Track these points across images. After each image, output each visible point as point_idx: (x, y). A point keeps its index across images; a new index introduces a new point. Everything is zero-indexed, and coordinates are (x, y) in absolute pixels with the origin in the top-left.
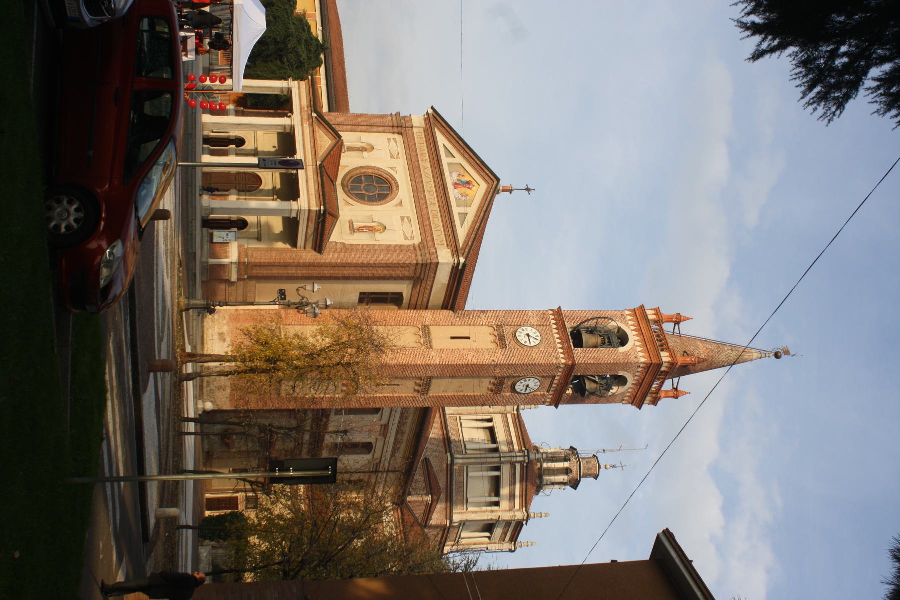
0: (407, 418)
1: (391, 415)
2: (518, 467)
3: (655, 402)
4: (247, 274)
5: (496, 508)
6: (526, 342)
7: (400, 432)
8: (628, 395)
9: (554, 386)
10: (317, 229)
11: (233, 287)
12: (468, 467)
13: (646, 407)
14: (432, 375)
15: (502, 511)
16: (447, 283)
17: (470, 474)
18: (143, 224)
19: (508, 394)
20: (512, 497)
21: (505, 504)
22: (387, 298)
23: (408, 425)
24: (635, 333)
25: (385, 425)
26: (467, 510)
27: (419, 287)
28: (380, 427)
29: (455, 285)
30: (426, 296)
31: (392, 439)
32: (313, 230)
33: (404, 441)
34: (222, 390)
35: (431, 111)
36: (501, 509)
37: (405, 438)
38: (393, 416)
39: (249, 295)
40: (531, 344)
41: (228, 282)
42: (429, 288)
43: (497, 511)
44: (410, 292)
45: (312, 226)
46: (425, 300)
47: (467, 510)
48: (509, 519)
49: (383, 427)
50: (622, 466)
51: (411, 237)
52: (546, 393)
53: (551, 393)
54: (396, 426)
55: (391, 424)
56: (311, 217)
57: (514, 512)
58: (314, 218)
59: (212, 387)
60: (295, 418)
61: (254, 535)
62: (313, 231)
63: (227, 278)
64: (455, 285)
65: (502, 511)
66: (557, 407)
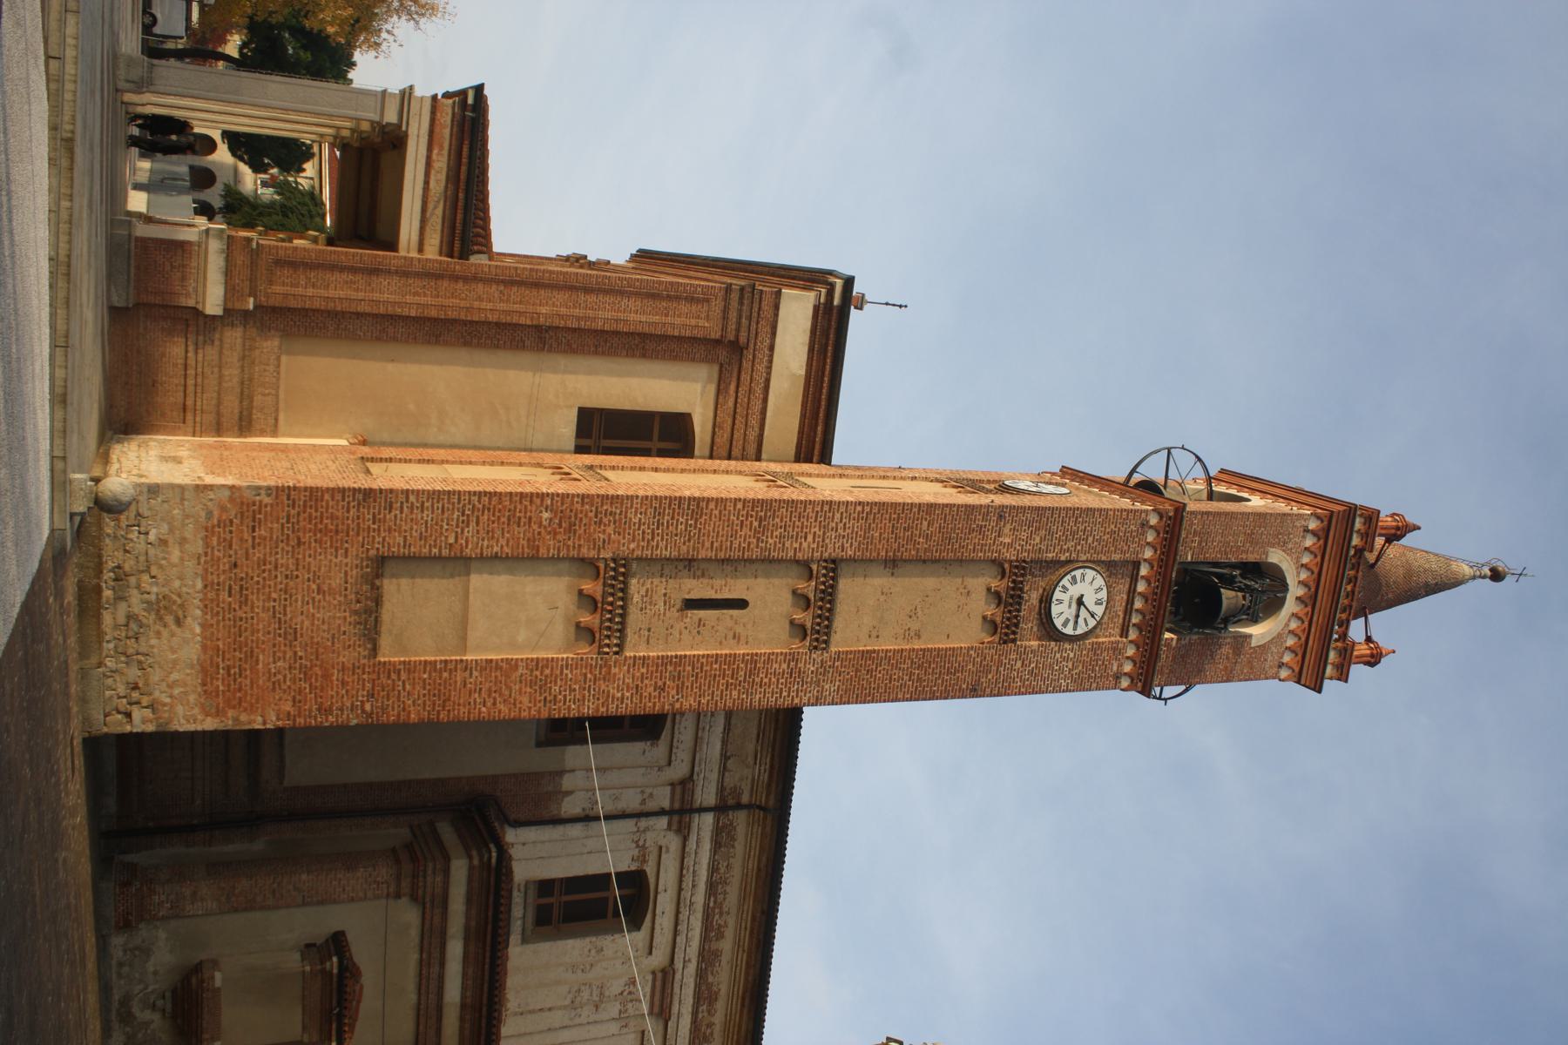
0: (720, 936)
3: (1343, 675)
4: (253, 293)
6: (1065, 624)
7: (704, 995)
8: (1290, 642)
9: (1138, 604)
10: (453, 177)
11: (209, 349)
13: (1328, 685)
14: (838, 554)
16: (803, 372)
19: (1035, 643)
22: (661, 439)
23: (724, 962)
24: (1301, 592)
25: (663, 971)
27: (733, 387)
28: (650, 977)
29: (828, 367)
30: (754, 422)
31: (686, 1022)
32: (443, 177)
33: (717, 1029)
34: (169, 619)
37: (718, 1019)
38: (682, 928)
39: (258, 400)
40: (1075, 629)
41: (194, 322)
42: (759, 391)
44: (711, 414)
45: (441, 163)
46: (752, 435)
49: (659, 975)
50: (1520, 575)
51: (587, 791)
52: (1118, 638)
53: (1133, 635)
54: (692, 968)
55: (678, 965)
56: (437, 130)
58: (447, 132)
59: (136, 603)
60: (414, 898)
62: (443, 184)
63: (191, 303)
64: (828, 367)
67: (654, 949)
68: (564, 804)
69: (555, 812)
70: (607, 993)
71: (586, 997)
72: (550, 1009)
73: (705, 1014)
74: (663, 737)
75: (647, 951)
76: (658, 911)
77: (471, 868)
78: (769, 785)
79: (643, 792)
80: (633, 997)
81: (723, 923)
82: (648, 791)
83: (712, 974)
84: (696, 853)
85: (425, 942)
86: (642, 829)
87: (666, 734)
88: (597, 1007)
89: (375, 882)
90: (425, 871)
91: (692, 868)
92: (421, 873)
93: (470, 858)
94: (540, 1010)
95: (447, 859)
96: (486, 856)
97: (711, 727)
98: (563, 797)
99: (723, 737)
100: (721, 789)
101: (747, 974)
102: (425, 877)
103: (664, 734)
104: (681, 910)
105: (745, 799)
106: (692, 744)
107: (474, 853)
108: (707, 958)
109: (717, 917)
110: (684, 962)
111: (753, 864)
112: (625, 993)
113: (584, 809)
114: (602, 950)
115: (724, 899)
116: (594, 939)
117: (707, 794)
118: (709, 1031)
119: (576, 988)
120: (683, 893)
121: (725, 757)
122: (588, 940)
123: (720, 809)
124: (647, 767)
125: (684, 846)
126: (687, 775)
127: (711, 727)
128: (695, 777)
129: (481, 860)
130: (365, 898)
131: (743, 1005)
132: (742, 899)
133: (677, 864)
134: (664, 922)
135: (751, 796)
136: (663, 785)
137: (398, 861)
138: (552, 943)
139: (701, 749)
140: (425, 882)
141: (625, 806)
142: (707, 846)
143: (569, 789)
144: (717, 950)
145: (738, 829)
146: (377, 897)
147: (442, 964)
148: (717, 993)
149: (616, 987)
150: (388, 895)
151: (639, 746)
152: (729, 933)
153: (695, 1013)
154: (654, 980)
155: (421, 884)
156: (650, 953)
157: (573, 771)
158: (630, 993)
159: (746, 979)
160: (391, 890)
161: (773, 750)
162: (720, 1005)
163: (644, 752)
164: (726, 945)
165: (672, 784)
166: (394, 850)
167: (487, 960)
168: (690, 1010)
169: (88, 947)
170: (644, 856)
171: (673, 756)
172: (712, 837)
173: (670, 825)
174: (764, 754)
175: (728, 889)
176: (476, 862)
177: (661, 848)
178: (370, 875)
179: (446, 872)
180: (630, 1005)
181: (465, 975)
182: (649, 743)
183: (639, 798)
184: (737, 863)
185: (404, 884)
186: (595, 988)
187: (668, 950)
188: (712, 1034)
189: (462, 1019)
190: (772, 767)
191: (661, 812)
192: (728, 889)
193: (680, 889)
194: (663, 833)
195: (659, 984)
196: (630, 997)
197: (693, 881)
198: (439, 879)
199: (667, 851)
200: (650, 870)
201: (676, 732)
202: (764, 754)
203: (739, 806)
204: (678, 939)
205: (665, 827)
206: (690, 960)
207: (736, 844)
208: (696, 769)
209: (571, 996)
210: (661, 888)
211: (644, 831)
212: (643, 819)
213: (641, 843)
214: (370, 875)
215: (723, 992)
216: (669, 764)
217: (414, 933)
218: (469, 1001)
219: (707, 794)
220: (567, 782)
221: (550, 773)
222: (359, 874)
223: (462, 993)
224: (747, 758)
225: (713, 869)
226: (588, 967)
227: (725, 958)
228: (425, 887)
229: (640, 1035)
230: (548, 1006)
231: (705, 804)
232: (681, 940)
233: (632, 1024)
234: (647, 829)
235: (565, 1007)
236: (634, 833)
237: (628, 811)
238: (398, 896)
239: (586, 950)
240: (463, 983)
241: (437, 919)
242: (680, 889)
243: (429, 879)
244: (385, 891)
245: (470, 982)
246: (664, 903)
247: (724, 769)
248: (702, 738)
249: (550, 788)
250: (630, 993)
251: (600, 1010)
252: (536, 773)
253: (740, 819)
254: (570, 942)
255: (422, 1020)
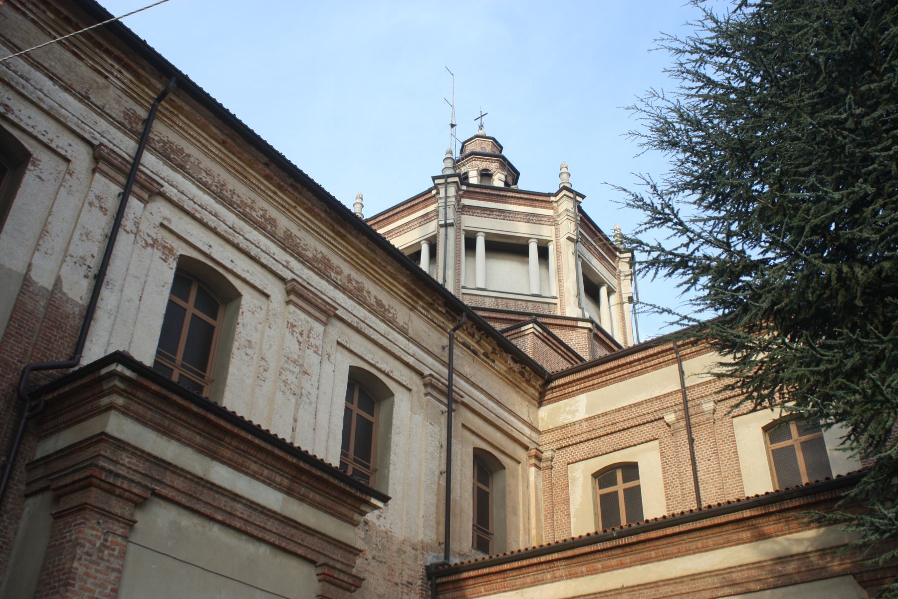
0: (273, 222)
1: (187, 213)
2: (466, 202)
5: (552, 248)
7: (322, 268)
12: (464, 287)
15: (557, 236)
17: (480, 285)
18: (808, 539)
20: (529, 218)
21: (547, 232)
25: (288, 292)
26: (555, 298)
28: (292, 308)
31: (341, 298)
33: (355, 275)
35: (320, 577)
36: (553, 238)
37: (347, 269)
38: (254, 251)
43: (558, 247)
47: (555, 298)
48: (573, 224)
49: (292, 297)
54: (295, 264)
55: (288, 275)
57: (559, 216)
60: (140, 503)
61: (761, 284)
65: (557, 236)
66: (389, 498)
67: (265, 291)
68: (70, 295)
69: (77, 310)
70: (296, 357)
71: (293, 379)
72: (295, 420)
73: (339, 277)
74: (30, 149)
75: (263, 299)
76: (229, 266)
77: (125, 412)
78: (137, 76)
79: (91, 204)
80: (305, 333)
81: (261, 212)
82: (91, 197)
83: (306, 250)
84: (182, 193)
85: (203, 509)
86: (135, 230)
87: (28, 144)
88: (305, 373)
89: (100, 550)
90: (110, 472)
91: (196, 206)
92: (111, 480)
93: (111, 407)
94: (293, 430)
95: (103, 437)
96: (117, 383)
97: (41, 90)
98: (61, 291)
99: (61, 86)
100: (120, 126)
101: (316, 215)
102: (117, 475)
103: (26, 145)
104: (236, 241)
105: (143, 114)
106: (52, 122)
107: (105, 401)
108: (288, 244)
109: (254, 214)
110: (287, 267)
111: (215, 147)
112: (300, 339)
113: (86, 277)
114: (250, 342)
115: (239, 196)
116: (236, 344)
117: (126, 145)
118: (354, 283)
119: (282, 384)
120: (219, 230)
121: (84, 99)
122: (234, 350)
123: (143, 141)
124: (61, 185)
125: (169, 200)
126: (91, 151)
127: (41, 90)
128: (96, 143)
129: (120, 393)
130: (119, 571)
131: (343, 237)
132: (244, 179)
133: (187, 219)
134: (242, 265)
135: (142, 105)
136: (92, 180)
137: (82, 508)
138: (227, 389)
139: (66, 118)
140: (124, 478)
141: (100, 231)
142: (178, 178)
143: (53, 282)
144: (285, 232)
145: (171, 139)
146: (123, 555)
147: (236, 497)
148: (324, 257)
149: (292, 345)
150: (125, 538)
151: (29, 178)
152: (273, 213)
153: (337, 286)
154: (296, 305)
155: (126, 485)
156: (267, 296)
157: (30, 265)
158: (301, 334)
159: (322, 220)
160: (120, 531)
161: (100, 46)
162: (336, 261)
163: (40, 178)
164: (284, 223)
165: (94, 171)
166: (57, 517)
167: (250, 437)
168: (332, 288)
169: (575, 378)
170: (165, 247)
171: (59, 150)
172: (171, 167)
173: (140, 199)
174: (98, 60)
175: (230, 187)
176: (120, 401)
177: (162, 225)
178: (88, 554)
179: (121, 445)
180: (311, 339)
181: (254, 476)
182: (30, 167)
183: (96, 211)
184: (207, 163)
185: (117, 510)
186: (286, 366)
187: (270, 277)
188: (357, 282)
189: (302, 499)
190: (118, 60)
191: (124, 200)
192: (230, 187)
193: (214, 231)
194: (147, 213)
195: (300, 302)
196: (305, 336)
197: (210, 213)
198: (126, 459)
199: (169, 220)
200: (183, 250)
201: (30, 130)
202: (98, 60)
203: (148, 123)
204: (263, 260)
205: (142, 205)
206: (288, 262)
207: (187, 151)
208: (87, 136)
209: (288, 393)
210: (205, 249)
211: (138, 231)
212: (123, 222)
213: (150, 241)
214: (88, 554)
215: (325, 251)
216: (68, 161)
217: (187, 521)
218: (286, 482)
219: (126, 145)
220: (43, 278)
221: (21, 292)
222: (82, 570)
223: (275, 488)
224: (97, 83)
225: (204, 186)
226: (263, 363)
227: (295, 230)
228: (132, 481)
229: (340, 348)
230: (292, 420)
231: (133, 152)
232: (265, 259)
233: (328, 349)
234: (137, 224)
235: (297, 405)
236: (135, 242)
237: (108, 231)
238: (131, 524)
239: (245, 357)
240: (264, 482)
241: (179, 483)
242: (214, 231)
243: (123, 472)
244: (119, 539)
245: (266, 472)
246: (223, 254)
247: (101, 112)
248: (52, 108)
249: (42, 303)
250: (301, 334)
251: (309, 371)
252: (14, 310)
253: (161, 130)
254: (232, 370)
255: (291, 547)
